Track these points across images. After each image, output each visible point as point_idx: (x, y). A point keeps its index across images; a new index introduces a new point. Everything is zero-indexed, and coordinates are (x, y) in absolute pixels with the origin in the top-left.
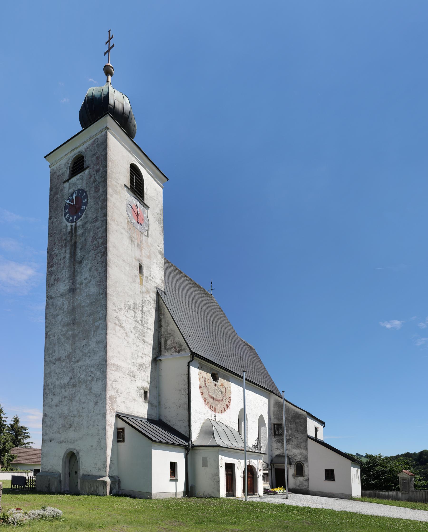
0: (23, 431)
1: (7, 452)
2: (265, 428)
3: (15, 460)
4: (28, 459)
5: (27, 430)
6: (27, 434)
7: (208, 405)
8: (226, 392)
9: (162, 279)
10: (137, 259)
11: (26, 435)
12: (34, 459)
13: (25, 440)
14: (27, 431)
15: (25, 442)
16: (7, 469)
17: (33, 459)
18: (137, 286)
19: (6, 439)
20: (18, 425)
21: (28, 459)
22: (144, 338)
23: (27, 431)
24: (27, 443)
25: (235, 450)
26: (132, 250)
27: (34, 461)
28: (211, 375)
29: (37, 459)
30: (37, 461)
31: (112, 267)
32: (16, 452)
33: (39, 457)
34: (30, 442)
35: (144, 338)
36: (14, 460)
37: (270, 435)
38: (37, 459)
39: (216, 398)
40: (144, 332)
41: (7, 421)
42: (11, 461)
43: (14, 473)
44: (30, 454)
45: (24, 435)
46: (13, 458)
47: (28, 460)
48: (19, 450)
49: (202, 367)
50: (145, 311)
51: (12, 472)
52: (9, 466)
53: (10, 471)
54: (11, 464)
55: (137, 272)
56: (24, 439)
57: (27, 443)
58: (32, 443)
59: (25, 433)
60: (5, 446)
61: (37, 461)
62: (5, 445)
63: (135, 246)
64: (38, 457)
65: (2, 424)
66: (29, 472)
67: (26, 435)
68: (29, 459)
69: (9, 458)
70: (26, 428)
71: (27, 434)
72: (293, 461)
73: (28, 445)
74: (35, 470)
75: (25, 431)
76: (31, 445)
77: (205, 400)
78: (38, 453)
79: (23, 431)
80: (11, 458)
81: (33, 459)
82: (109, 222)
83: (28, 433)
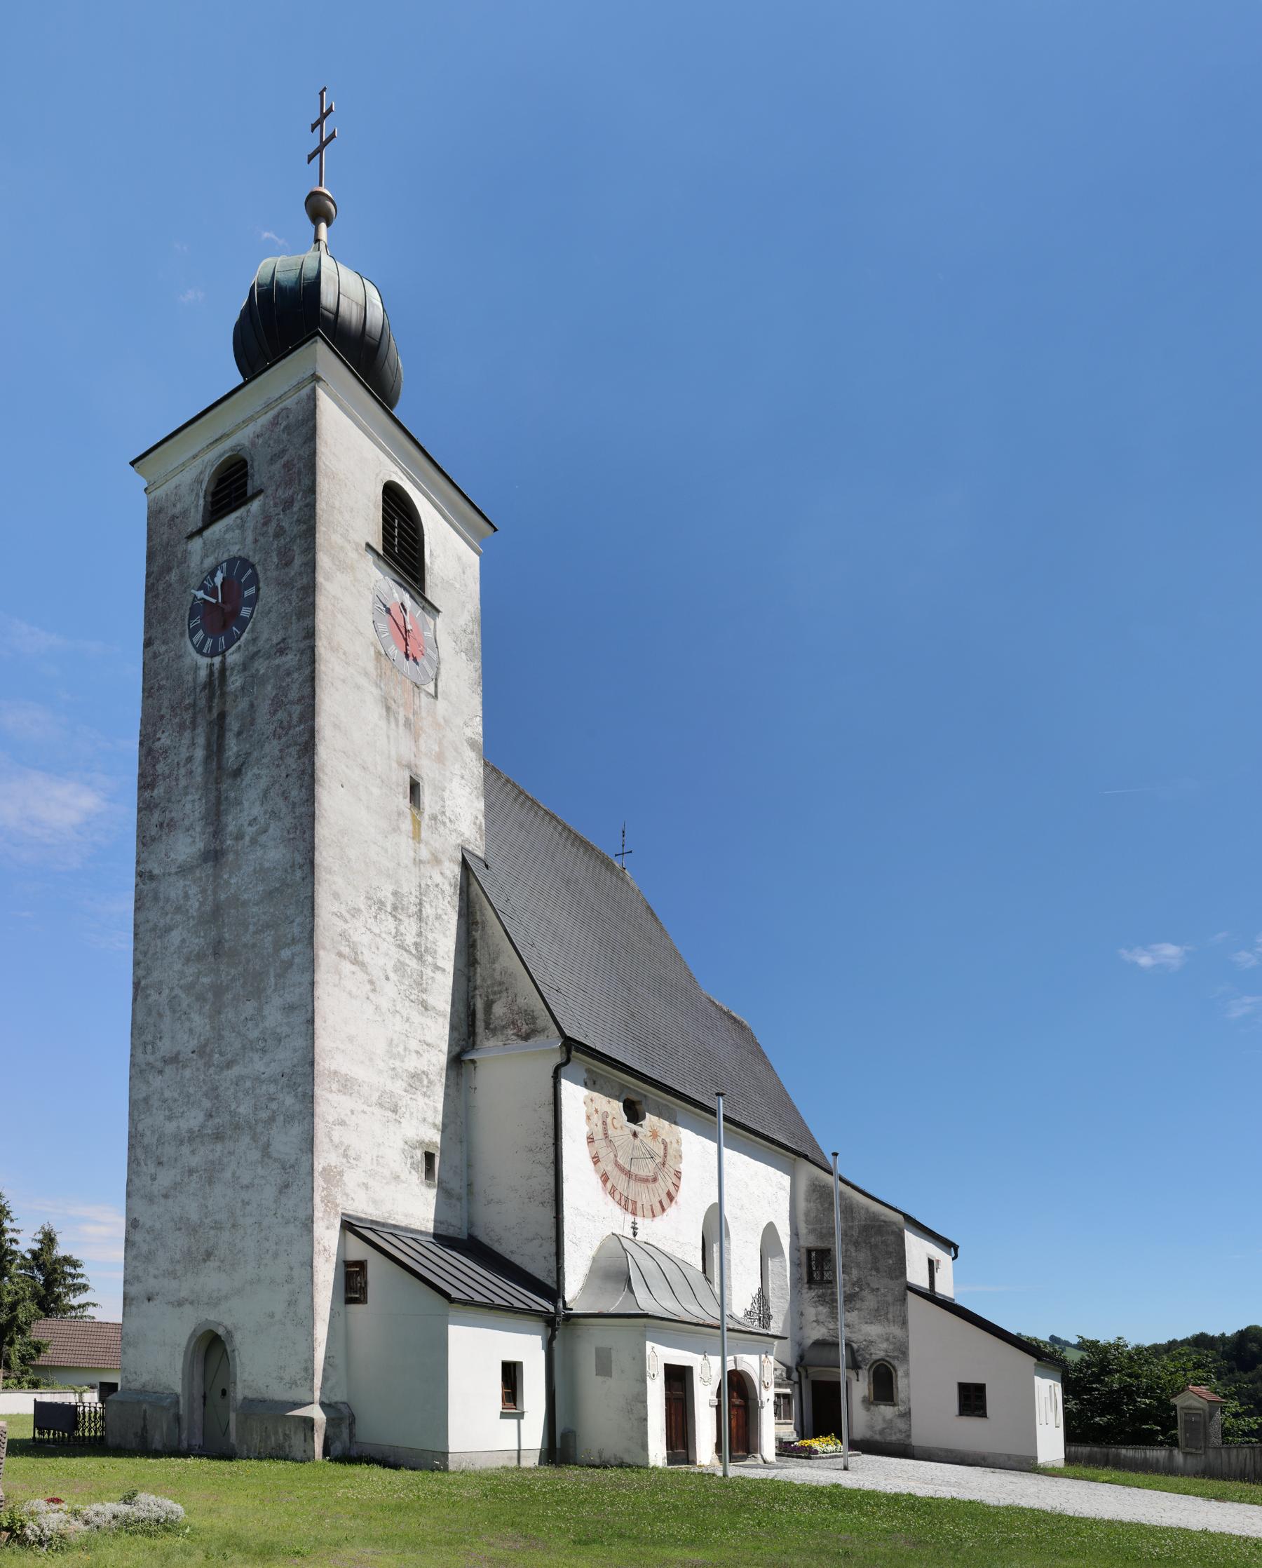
0: (68, 1269)
1: (21, 1331)
2: (781, 1262)
3: (45, 1355)
4: (83, 1353)
5: (80, 1266)
6: (80, 1281)
7: (612, 1193)
8: (665, 1157)
9: (478, 822)
10: (404, 763)
11: (75, 1281)
12: (101, 1354)
13: (74, 1297)
14: (79, 1270)
15: (75, 1302)
16: (19, 1383)
17: (98, 1353)
18: (405, 844)
19: (16, 1293)
20: (54, 1252)
21: (83, 1353)
22: (424, 996)
23: (79, 1270)
24: (79, 1306)
25: (693, 1327)
26: (388, 737)
27: (101, 1358)
28: (621, 1104)
29: (111, 1354)
30: (110, 1358)
31: (330, 787)
32: (47, 1331)
33: (115, 1346)
34: (88, 1304)
35: (424, 996)
36: (42, 1354)
37: (795, 1282)
38: (111, 1354)
39: (636, 1172)
40: (424, 978)
41: (19, 1241)
42: (32, 1358)
43: (41, 1393)
44: (89, 1337)
45: (69, 1281)
46: (38, 1350)
47: (82, 1357)
48: (57, 1327)
49: (594, 1083)
50: (428, 917)
51: (35, 1391)
52: (26, 1372)
53: (29, 1388)
54: (32, 1366)
55: (404, 802)
56: (71, 1295)
57: (81, 1306)
58: (94, 1305)
59: (73, 1276)
60: (14, 1313)
61: (110, 1358)
62: (15, 1310)
63: (397, 725)
64: (112, 1346)
65: (7, 1249)
66: (84, 1391)
67: (75, 1281)
68: (86, 1353)
69: (27, 1351)
70: (78, 1261)
71: (80, 1281)
72: (864, 1359)
73: (84, 1311)
74: (102, 1384)
75: (73, 1271)
76: (90, 1311)
77: (605, 1178)
78: (113, 1335)
79: (68, 1269)
80: (33, 1351)
81: (98, 1353)
82: (320, 654)
83: (82, 1276)
